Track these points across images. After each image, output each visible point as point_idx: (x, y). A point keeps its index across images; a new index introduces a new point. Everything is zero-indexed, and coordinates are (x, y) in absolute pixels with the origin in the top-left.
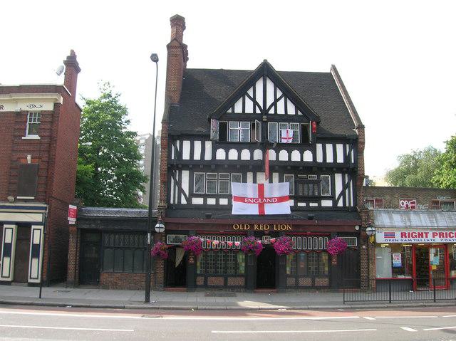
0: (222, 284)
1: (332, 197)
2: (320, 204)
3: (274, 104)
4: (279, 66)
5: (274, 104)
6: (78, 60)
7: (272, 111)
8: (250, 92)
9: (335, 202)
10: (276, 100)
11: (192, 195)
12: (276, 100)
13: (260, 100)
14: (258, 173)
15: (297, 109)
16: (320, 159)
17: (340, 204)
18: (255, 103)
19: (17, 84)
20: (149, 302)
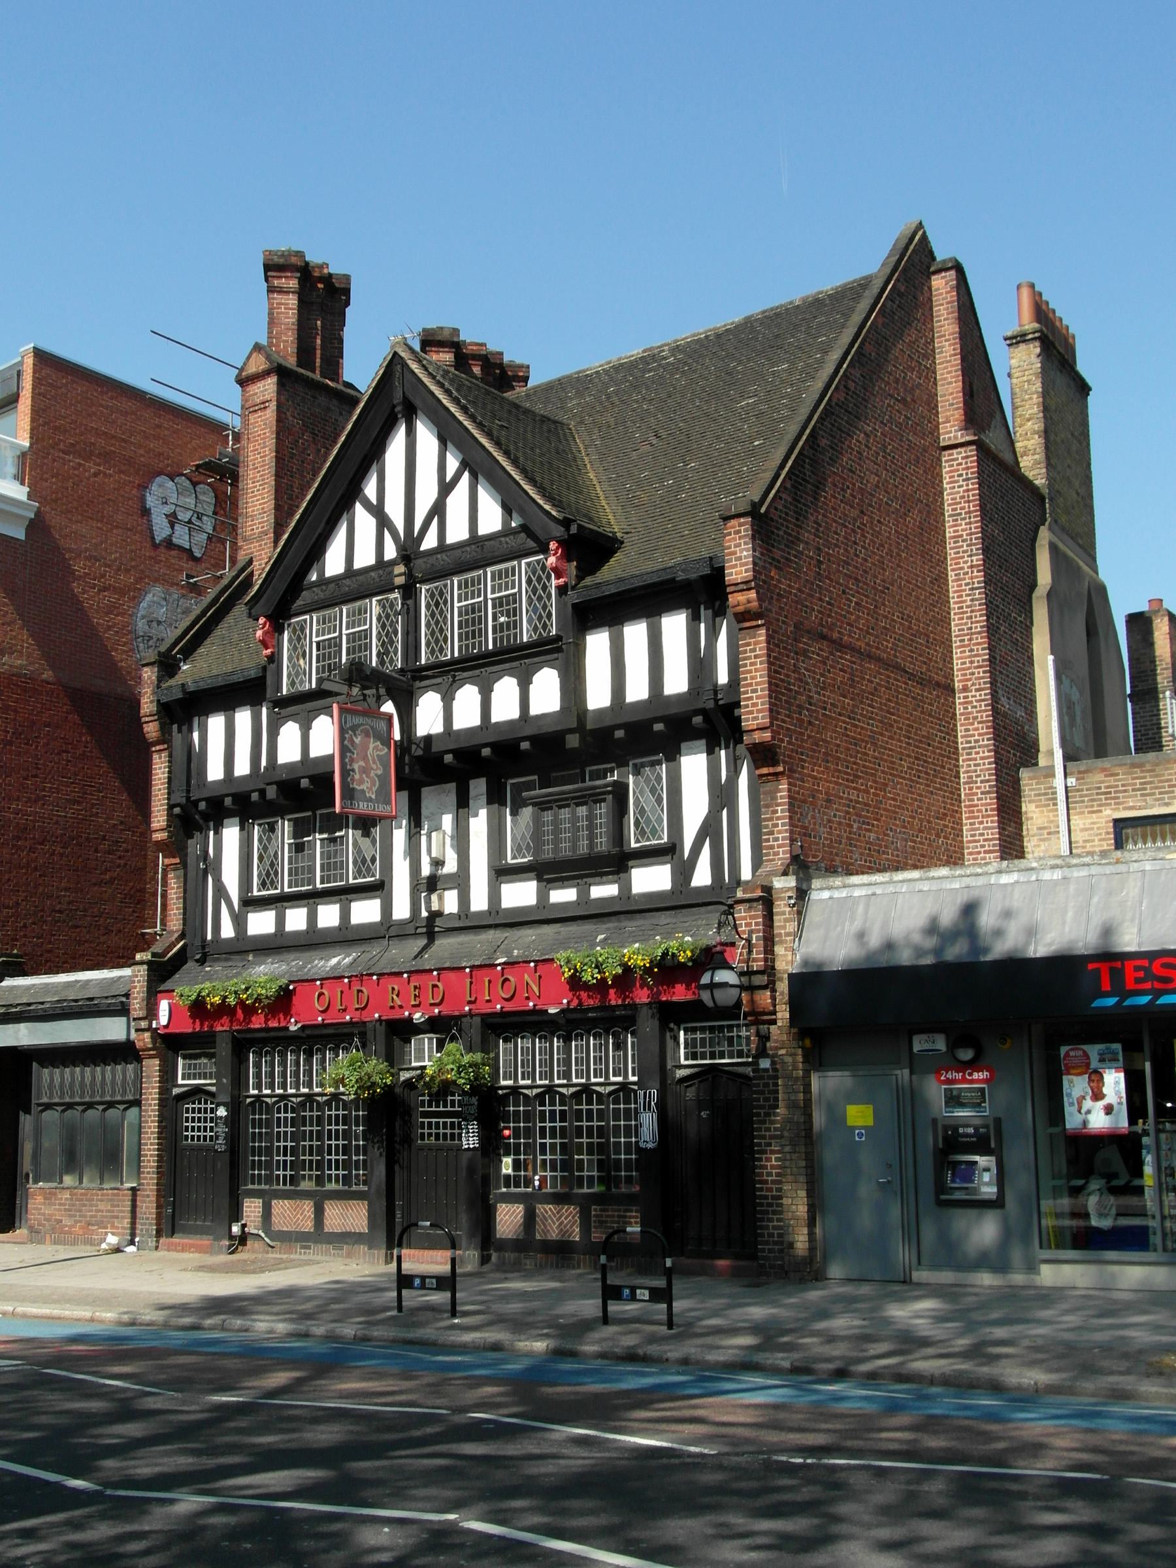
0: (308, 1226)
1: (668, 852)
2: (626, 887)
3: (438, 510)
4: (466, 336)
5: (438, 510)
6: (930, 239)
7: (430, 542)
8: (370, 490)
9: (683, 872)
10: (446, 488)
11: (250, 903)
12: (446, 488)
13: (395, 510)
14: (425, 791)
15: (507, 509)
16: (598, 697)
17: (702, 876)
18: (383, 522)
19: (972, 290)
20: (1021, 854)
